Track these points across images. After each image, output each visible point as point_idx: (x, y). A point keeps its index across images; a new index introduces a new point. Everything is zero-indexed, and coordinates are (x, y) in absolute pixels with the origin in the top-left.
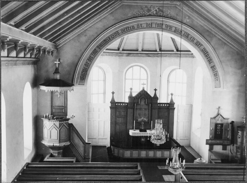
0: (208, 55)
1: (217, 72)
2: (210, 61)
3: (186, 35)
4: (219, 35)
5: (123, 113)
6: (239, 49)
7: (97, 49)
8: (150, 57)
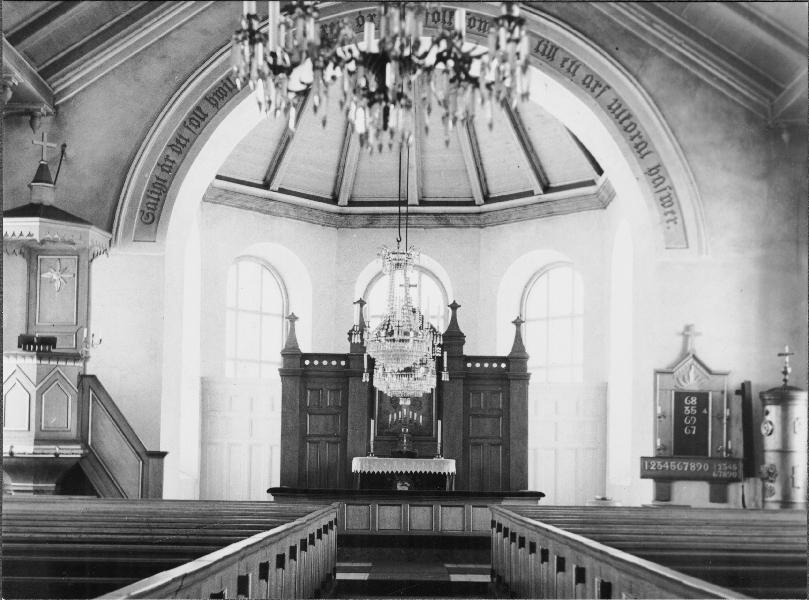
0: (632, 127)
1: (670, 188)
2: (640, 147)
3: (546, 53)
4: (671, 49)
5: (329, 399)
6: (754, 99)
7: (207, 108)
8: (453, 226)
